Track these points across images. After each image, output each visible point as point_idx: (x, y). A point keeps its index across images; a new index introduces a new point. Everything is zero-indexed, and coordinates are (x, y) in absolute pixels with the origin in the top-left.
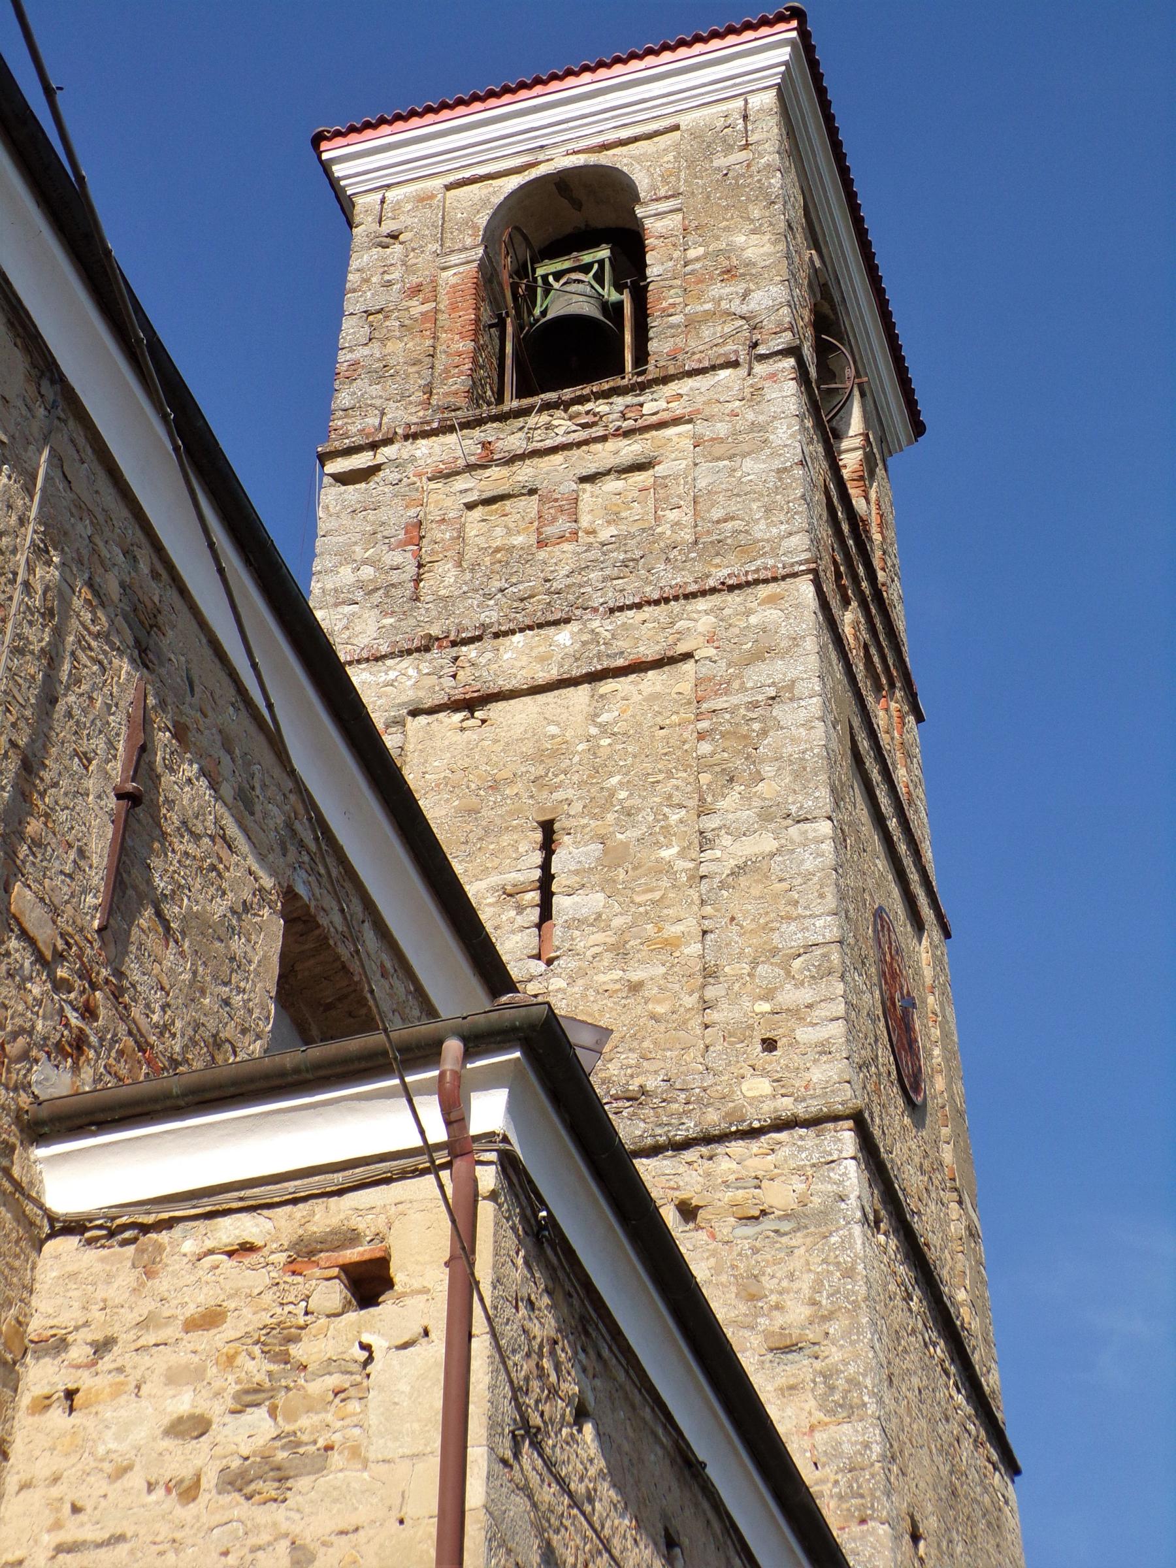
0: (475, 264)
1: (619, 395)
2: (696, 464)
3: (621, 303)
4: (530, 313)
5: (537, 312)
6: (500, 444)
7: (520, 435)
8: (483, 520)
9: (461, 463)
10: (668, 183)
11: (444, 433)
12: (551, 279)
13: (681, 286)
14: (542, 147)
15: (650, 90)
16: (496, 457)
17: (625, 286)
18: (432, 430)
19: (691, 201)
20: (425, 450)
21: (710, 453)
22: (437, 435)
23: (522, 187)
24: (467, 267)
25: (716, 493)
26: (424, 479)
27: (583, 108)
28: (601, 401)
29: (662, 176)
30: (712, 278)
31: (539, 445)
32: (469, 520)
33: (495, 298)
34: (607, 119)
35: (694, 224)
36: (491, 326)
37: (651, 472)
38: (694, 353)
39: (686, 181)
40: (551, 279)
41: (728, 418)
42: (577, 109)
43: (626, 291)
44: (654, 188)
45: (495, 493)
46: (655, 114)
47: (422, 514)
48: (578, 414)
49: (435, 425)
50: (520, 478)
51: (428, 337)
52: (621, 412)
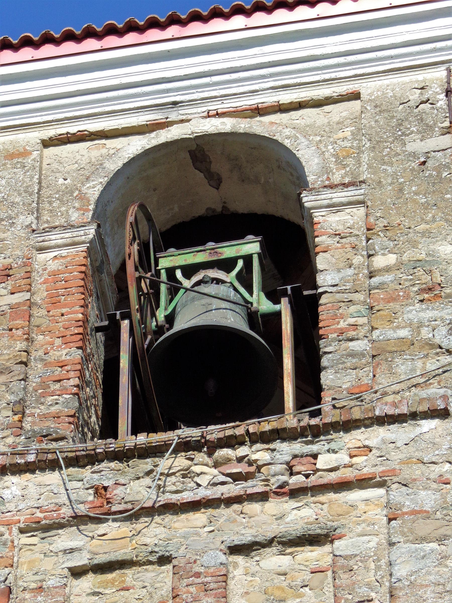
0: (83, 248)
1: (284, 440)
2: (391, 544)
3: (278, 314)
4: (153, 315)
5: (161, 315)
6: (119, 491)
7: (147, 481)
8: (95, 594)
9: (66, 512)
10: (344, 167)
11: (43, 470)
12: (179, 274)
13: (364, 303)
14: (175, 103)
15: (322, 46)
16: (114, 509)
17: (284, 293)
18: (27, 464)
19: (378, 193)
20: (16, 491)
21: (411, 531)
22: (33, 472)
23: (147, 153)
24: (72, 250)
25: (422, 586)
26: (15, 530)
27: (233, 59)
28: (259, 446)
29: (336, 156)
30: (407, 297)
31: (175, 498)
32: (76, 591)
33: (103, 293)
34: (263, 77)
35: (381, 223)
36: (98, 329)
37: (327, 548)
38: (385, 394)
39: (370, 166)
40: (179, 274)
41: (434, 486)
42: (225, 61)
43: (285, 301)
44: (326, 170)
45: (112, 557)
46: (327, 77)
47: (11, 577)
48: (228, 460)
49: (31, 458)
50: (147, 540)
51: (20, 339)
52: (288, 463)
